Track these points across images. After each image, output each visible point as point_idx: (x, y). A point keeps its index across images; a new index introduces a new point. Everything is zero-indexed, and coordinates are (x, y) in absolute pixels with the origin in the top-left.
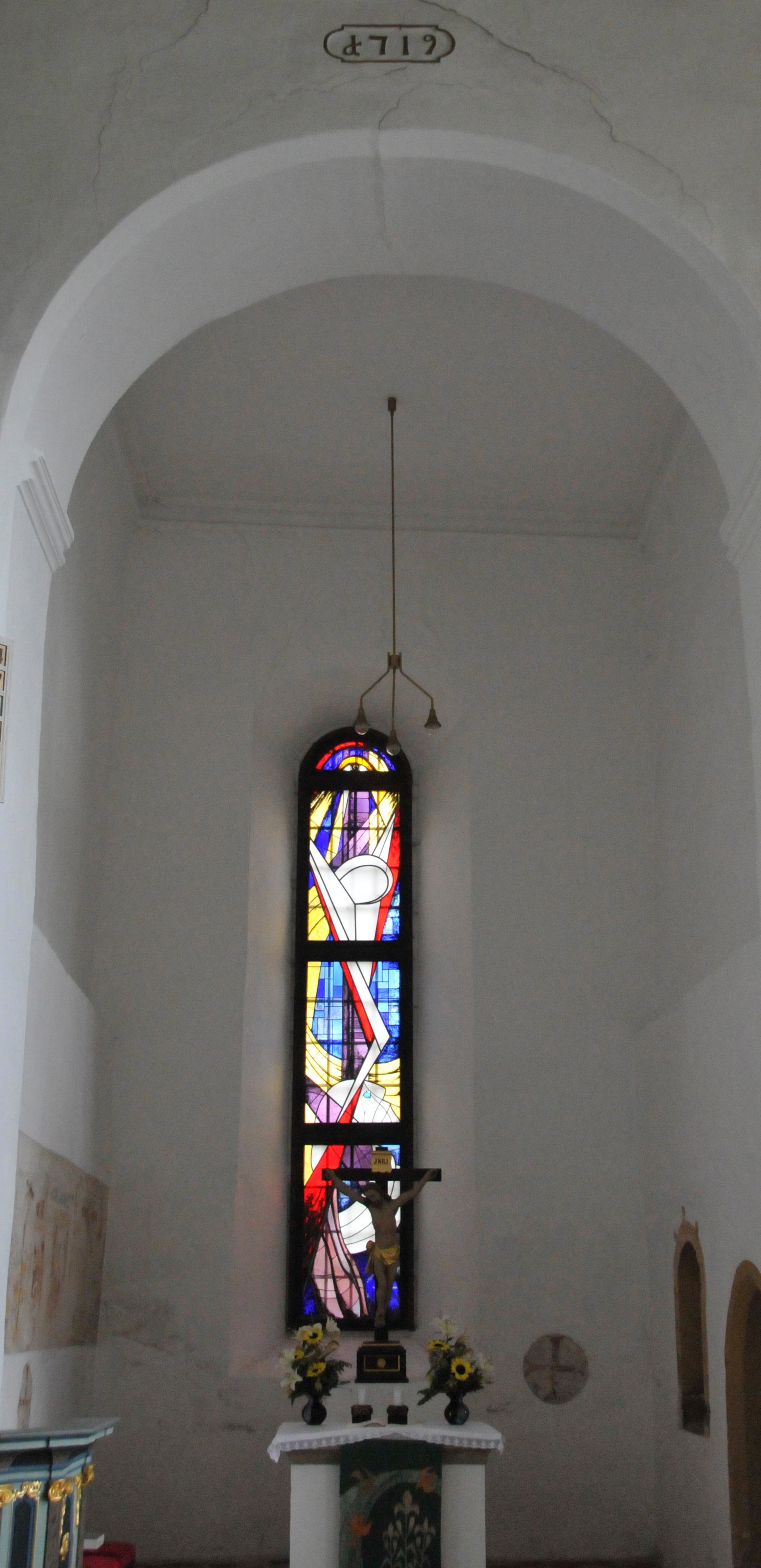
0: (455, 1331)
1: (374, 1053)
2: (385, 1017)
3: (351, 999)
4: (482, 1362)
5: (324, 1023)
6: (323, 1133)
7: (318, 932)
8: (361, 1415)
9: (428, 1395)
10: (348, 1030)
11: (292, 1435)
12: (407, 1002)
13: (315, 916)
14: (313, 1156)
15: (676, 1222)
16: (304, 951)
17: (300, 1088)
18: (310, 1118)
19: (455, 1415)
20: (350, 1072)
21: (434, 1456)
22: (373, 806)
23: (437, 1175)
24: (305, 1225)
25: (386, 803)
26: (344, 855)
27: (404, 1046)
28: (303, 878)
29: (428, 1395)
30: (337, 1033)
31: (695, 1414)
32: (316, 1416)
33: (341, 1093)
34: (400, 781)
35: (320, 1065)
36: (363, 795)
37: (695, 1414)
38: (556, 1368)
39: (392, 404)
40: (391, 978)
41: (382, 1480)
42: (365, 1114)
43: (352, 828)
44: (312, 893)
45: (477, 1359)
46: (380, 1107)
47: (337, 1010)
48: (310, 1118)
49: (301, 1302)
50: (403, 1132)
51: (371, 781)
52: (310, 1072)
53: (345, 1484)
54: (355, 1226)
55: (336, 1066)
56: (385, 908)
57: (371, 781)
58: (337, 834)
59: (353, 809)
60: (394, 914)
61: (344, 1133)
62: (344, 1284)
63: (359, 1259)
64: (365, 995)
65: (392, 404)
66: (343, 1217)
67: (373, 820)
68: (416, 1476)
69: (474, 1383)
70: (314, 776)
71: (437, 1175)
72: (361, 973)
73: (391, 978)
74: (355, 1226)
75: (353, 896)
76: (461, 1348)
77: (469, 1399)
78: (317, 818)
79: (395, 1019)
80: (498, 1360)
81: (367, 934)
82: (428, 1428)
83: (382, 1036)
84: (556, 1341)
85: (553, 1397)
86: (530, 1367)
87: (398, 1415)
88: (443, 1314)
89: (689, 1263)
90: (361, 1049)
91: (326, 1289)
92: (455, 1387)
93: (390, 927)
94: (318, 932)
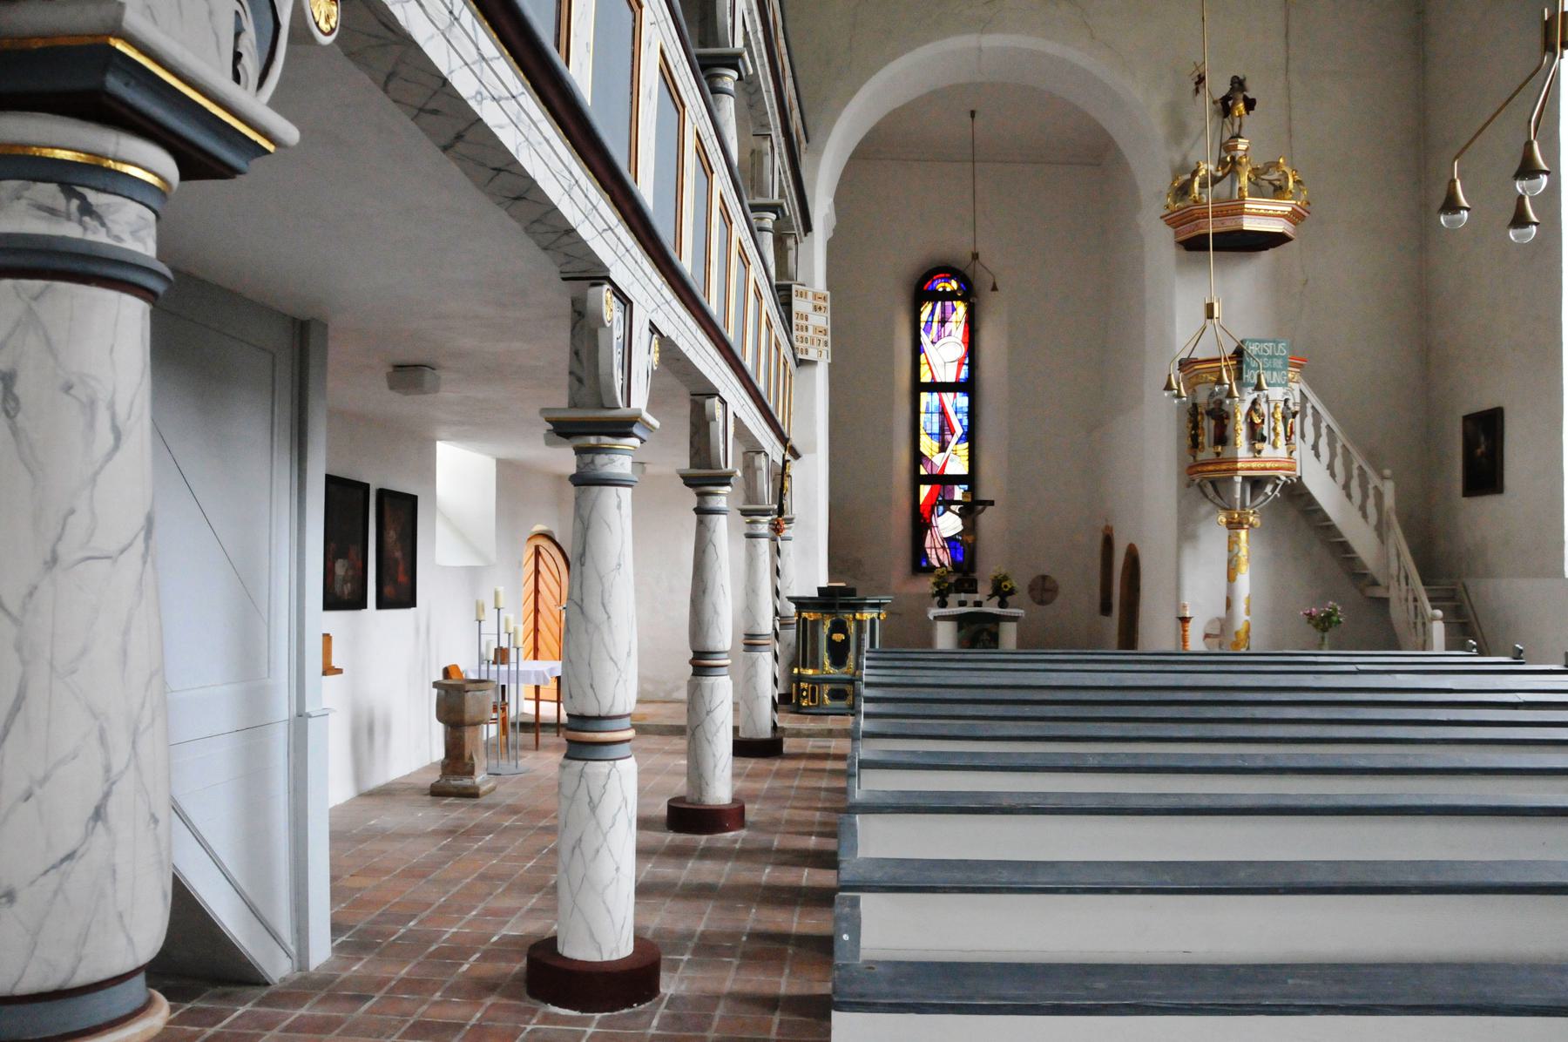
0: (1003, 571)
1: (955, 439)
2: (960, 421)
3: (943, 412)
4: (1015, 584)
5: (930, 422)
6: (928, 479)
7: (925, 377)
8: (962, 604)
9: (991, 596)
10: (942, 428)
11: (934, 612)
12: (972, 413)
13: (924, 370)
14: (925, 490)
15: (1103, 526)
16: (918, 387)
17: (918, 457)
18: (923, 472)
19: (1002, 605)
20: (943, 449)
21: (997, 619)
22: (954, 309)
23: (992, 503)
24: (921, 524)
25: (961, 308)
26: (939, 337)
27: (970, 436)
28: (917, 349)
29: (991, 596)
30: (936, 429)
31: (1106, 608)
32: (943, 604)
33: (938, 459)
34: (968, 294)
35: (928, 445)
36: (948, 303)
37: (1106, 608)
38: (1043, 590)
39: (973, 114)
40: (963, 401)
41: (975, 628)
42: (949, 471)
43: (943, 322)
44: (922, 357)
45: (1013, 583)
46: (957, 464)
47: (936, 418)
48: (923, 472)
49: (919, 562)
50: (970, 479)
51: (951, 296)
52: (922, 449)
53: (960, 628)
54: (948, 524)
55: (936, 445)
56: (961, 364)
57: (951, 296)
58: (935, 325)
59: (943, 312)
60: (965, 368)
61: (943, 481)
62: (940, 551)
63: (950, 540)
64: (950, 410)
65: (973, 114)
66: (940, 520)
67: (954, 317)
68: (988, 626)
69: (1011, 592)
70: (922, 293)
71: (992, 503)
72: (948, 398)
73: (963, 401)
74: (948, 524)
75: (944, 356)
76: (1005, 578)
77: (1009, 599)
78: (924, 317)
79: (965, 422)
80: (1019, 582)
81: (952, 379)
82: (992, 608)
83: (959, 431)
84: (1044, 578)
85: (1042, 602)
86: (1031, 589)
87: (978, 604)
88: (989, 566)
89: (1108, 543)
90: (948, 437)
91: (932, 554)
92: (1002, 592)
93: (964, 374)
94: (925, 377)
